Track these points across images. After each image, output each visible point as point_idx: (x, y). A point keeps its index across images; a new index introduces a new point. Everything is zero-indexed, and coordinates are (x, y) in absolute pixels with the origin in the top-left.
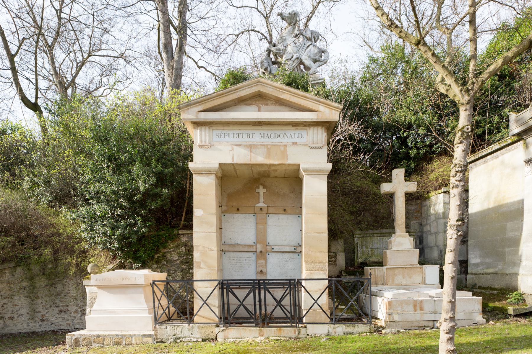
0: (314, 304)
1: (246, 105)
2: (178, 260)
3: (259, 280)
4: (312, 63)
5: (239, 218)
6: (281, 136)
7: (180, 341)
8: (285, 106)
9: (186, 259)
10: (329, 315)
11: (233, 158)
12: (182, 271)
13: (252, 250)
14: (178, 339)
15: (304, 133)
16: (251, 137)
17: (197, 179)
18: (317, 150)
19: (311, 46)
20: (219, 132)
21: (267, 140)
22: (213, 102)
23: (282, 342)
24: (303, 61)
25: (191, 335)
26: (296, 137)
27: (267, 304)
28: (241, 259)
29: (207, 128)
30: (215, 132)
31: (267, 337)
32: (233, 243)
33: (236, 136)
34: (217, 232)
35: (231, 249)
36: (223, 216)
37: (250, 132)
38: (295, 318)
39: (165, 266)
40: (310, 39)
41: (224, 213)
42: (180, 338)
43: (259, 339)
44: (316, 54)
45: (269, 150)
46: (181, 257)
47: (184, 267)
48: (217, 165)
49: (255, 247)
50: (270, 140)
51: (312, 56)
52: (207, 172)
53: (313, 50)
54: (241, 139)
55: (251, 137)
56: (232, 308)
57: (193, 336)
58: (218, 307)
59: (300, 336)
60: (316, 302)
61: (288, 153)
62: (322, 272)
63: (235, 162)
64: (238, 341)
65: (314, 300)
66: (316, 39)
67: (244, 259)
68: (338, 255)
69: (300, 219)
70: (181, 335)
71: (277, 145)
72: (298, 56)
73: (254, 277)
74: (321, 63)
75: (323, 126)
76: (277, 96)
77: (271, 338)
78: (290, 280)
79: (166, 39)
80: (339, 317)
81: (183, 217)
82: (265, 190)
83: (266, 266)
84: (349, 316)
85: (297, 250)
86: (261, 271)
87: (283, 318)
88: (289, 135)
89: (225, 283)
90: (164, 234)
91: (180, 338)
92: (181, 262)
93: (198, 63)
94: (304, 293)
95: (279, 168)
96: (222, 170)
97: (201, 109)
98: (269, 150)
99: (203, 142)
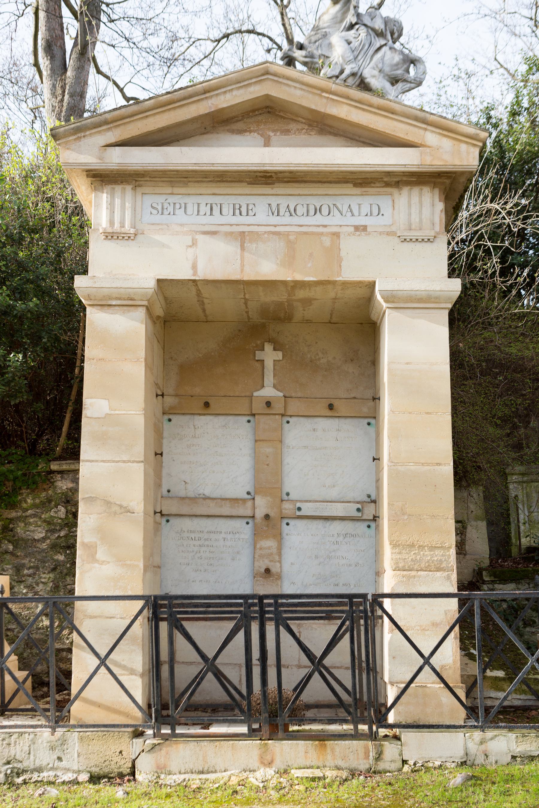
0: (421, 669)
1: (233, 132)
2: (44, 539)
3: (261, 598)
4: (388, 85)
5: (208, 427)
6: (325, 211)
7: (25, 782)
8: (335, 135)
9: (66, 536)
10: (462, 695)
11: (194, 267)
12: (54, 570)
13: (241, 511)
14: (18, 775)
15: (385, 202)
16: (244, 212)
17: (94, 318)
18: (419, 245)
19: (384, 49)
20: (160, 199)
21: (287, 219)
22: (145, 121)
23: (330, 785)
24: (368, 80)
25: (57, 763)
26: (363, 213)
27: (283, 662)
28: (212, 536)
29: (129, 188)
30: (149, 200)
31: (282, 768)
32: (191, 494)
33: (205, 209)
34: (145, 461)
35: (185, 510)
36: (166, 422)
37: (243, 201)
38: (363, 707)
39: (8, 557)
40: (380, 34)
41: (168, 413)
42: (24, 771)
43: (260, 774)
44: (397, 64)
45: (291, 244)
46: (53, 531)
47: (61, 558)
48: (152, 284)
49: (250, 503)
50: (295, 220)
51: (387, 69)
52: (124, 302)
53: (389, 57)
54: (217, 218)
55: (244, 212)
56: (185, 674)
57: (64, 764)
58: (142, 675)
59: (381, 766)
60: (427, 661)
61: (343, 254)
62: (439, 574)
63: (201, 275)
64: (195, 781)
65: (422, 655)
66: (396, 35)
67: (223, 535)
68: (469, 528)
69: (371, 430)
70: (28, 764)
71: (313, 233)
72: (355, 70)
73: (246, 589)
74: (409, 85)
75: (435, 185)
76: (313, 107)
77: (296, 773)
78: (351, 597)
79: (49, 29)
80: (497, 703)
81: (65, 429)
82: (279, 355)
83: (280, 554)
84: (517, 700)
85: (366, 513)
86: (268, 571)
87: (329, 706)
88: (345, 209)
89: (164, 606)
90: (12, 471)
91: (24, 771)
92: (54, 547)
93: (125, 90)
94: (388, 635)
95: (317, 293)
96: (166, 299)
97: (113, 140)
98: (291, 246)
99: (117, 226)
